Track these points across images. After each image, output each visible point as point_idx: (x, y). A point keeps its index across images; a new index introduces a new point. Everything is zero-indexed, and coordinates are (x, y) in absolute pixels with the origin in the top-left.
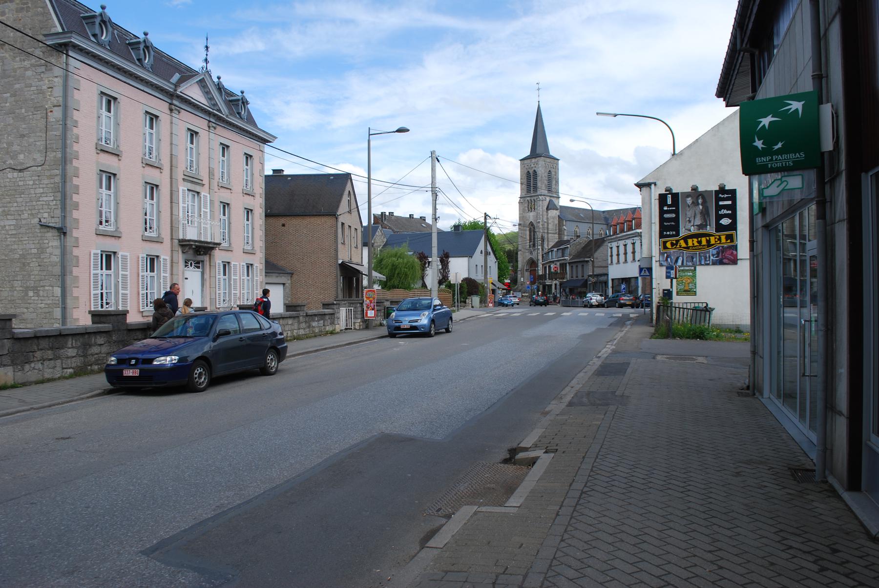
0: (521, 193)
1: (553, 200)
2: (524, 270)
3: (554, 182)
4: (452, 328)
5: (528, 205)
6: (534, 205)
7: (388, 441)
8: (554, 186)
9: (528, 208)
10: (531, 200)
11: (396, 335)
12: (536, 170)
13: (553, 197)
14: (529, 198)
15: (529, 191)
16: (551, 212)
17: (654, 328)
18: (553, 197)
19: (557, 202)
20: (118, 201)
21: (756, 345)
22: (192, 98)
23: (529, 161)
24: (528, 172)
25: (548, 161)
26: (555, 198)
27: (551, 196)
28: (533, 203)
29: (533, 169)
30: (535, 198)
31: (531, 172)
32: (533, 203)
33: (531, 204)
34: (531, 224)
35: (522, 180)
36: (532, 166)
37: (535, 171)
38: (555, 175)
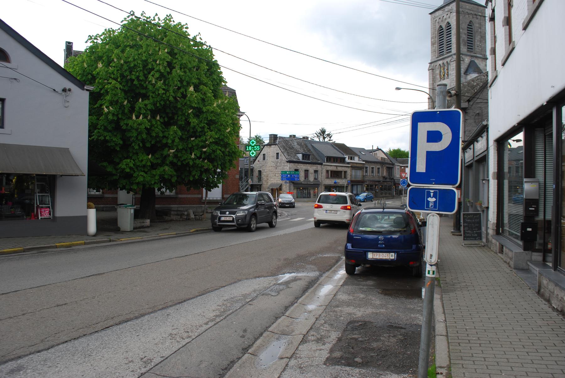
0: (432, 57)
1: (476, 61)
3: (478, 38)
4: (276, 223)
5: (440, 72)
6: (448, 69)
7: (398, 374)
8: (477, 43)
9: (440, 75)
10: (443, 63)
11: (221, 228)
12: (450, 22)
13: (476, 57)
14: (441, 62)
15: (441, 52)
17: (437, 366)
18: (476, 57)
19: (484, 65)
20: (328, 212)
21: (74, 247)
22: (338, 150)
23: (440, 12)
24: (441, 27)
25: (467, 7)
26: (480, 60)
27: (472, 56)
28: (446, 68)
29: (446, 21)
30: (448, 60)
31: (444, 25)
32: (446, 68)
33: (444, 69)
37: (448, 23)
38: (480, 28)
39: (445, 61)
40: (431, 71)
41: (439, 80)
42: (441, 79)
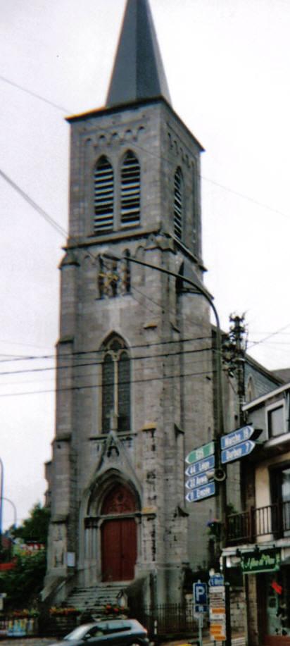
2: (77, 520)
16: (191, 300)
23: (106, 121)
34: (114, 340)
35: (76, 189)
36: (121, 134)
40: (69, 269)
41: (97, 295)
42: (101, 292)
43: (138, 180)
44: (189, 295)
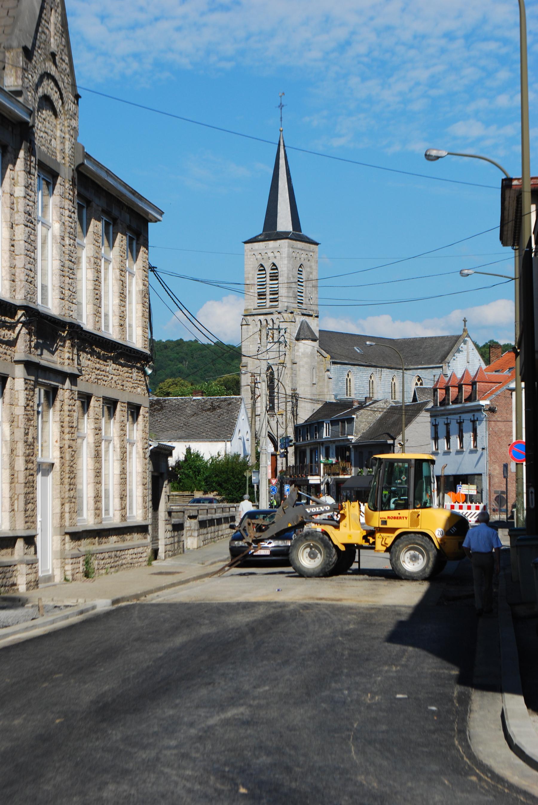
14: (262, 318)
39: (269, 317)
43: (277, 280)
44: (303, 341)
